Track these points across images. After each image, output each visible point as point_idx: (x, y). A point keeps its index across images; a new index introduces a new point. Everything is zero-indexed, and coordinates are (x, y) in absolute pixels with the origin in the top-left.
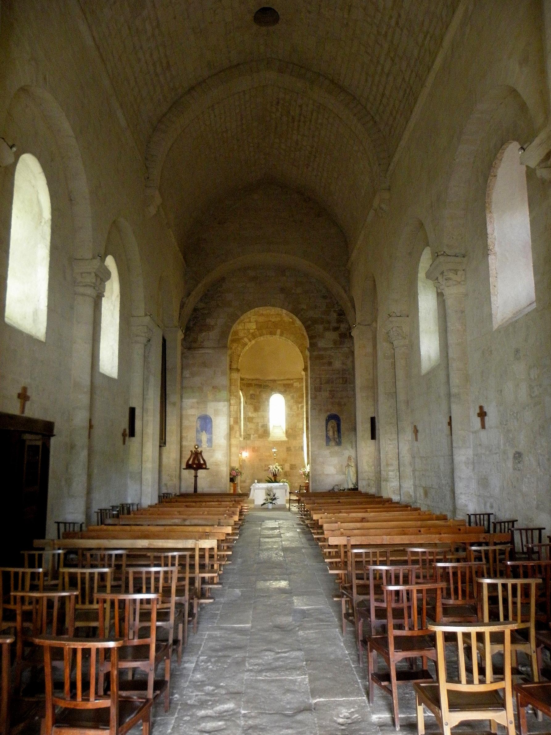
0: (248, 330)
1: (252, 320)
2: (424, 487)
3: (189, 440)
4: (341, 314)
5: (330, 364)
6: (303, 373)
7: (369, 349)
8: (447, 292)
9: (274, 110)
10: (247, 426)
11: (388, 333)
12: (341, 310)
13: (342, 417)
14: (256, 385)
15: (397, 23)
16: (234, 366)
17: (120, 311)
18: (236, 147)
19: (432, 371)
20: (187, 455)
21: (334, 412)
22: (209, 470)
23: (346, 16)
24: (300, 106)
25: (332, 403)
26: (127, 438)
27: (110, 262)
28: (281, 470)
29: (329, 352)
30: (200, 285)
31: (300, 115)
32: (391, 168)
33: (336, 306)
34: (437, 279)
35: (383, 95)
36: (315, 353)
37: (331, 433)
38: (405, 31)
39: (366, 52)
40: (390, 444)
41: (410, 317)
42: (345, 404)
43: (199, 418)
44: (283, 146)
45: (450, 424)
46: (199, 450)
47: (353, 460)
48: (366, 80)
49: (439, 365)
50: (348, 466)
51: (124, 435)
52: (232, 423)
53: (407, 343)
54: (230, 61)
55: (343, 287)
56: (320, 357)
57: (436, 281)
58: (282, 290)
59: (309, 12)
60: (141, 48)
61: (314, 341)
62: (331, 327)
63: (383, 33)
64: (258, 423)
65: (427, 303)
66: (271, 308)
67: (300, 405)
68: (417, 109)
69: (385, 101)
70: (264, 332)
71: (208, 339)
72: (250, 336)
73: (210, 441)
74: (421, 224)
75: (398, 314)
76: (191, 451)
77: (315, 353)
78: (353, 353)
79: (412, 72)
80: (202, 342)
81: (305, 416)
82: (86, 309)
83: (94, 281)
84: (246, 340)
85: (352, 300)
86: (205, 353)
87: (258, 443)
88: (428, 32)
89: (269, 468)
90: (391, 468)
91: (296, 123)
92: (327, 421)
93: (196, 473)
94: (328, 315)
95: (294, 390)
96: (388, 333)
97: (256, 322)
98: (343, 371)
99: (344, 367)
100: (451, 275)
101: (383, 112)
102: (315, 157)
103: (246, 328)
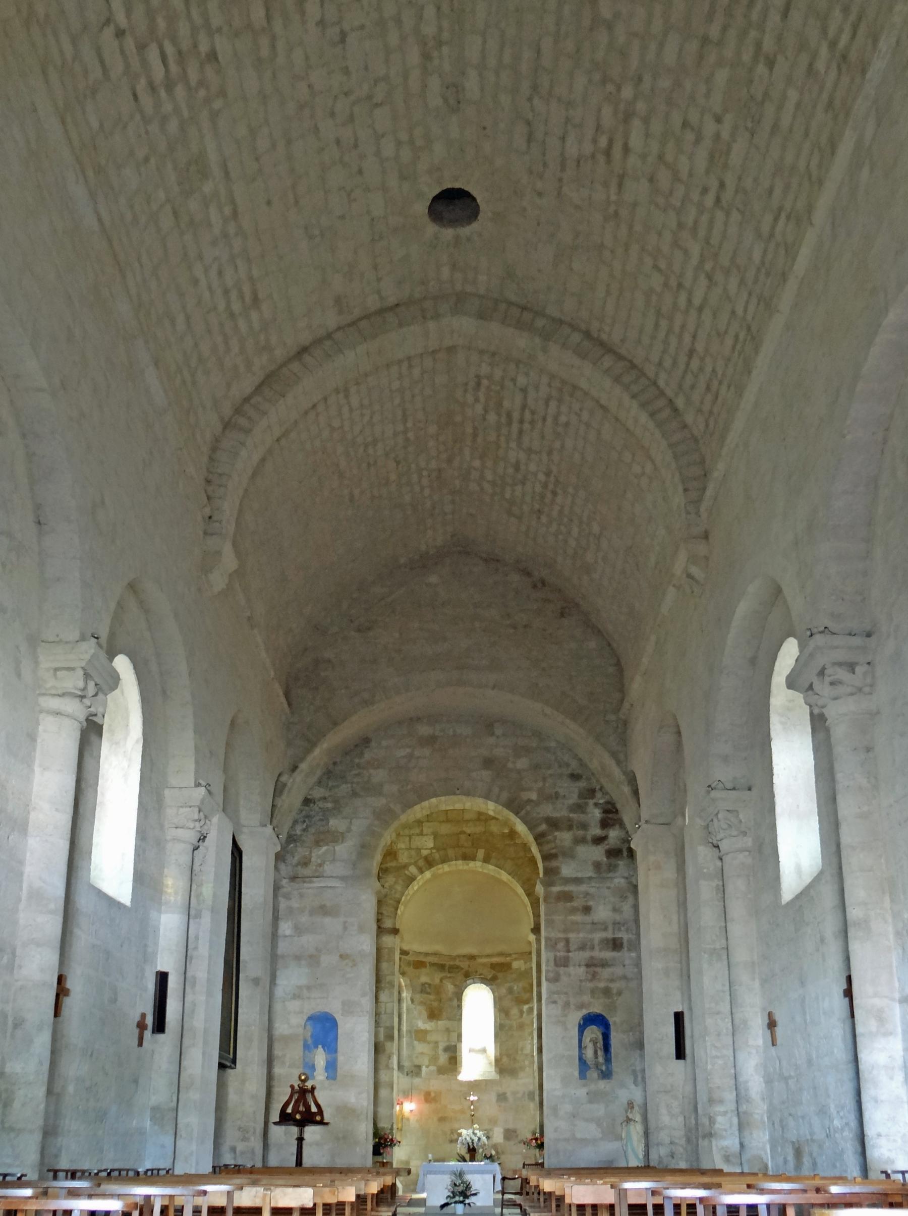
0: (418, 850)
1: (425, 831)
2: (793, 1143)
3: (287, 1064)
4: (611, 815)
5: (587, 910)
6: (532, 937)
7: (670, 873)
8: (833, 711)
9: (470, 399)
10: (413, 1047)
11: (707, 826)
12: (608, 803)
13: (614, 1020)
14: (433, 965)
15: (718, 200)
16: (388, 924)
17: (141, 770)
18: (393, 477)
19: (806, 894)
20: (282, 1095)
21: (597, 1009)
22: (330, 1126)
23: (613, 198)
24: (524, 391)
25: (593, 992)
26: (148, 1034)
27: (122, 664)
28: (484, 1139)
29: (583, 888)
30: (317, 752)
31: (524, 407)
32: (709, 492)
33: (599, 795)
34: (811, 687)
35: (691, 353)
36: (556, 889)
37: (589, 1053)
38: (735, 216)
39: (656, 267)
40: (717, 1057)
41: (755, 791)
42: (619, 993)
43: (310, 1018)
44: (489, 476)
45: (848, 993)
46: (309, 1084)
47: (636, 1108)
48: (657, 325)
49: (821, 873)
50: (628, 1120)
51: (141, 1026)
52: (382, 1037)
53: (750, 844)
54: (381, 298)
55: (614, 755)
56: (567, 897)
57: (810, 692)
58: (488, 763)
59: (540, 194)
60: (200, 257)
61: (554, 864)
62: (589, 838)
63: (690, 223)
64: (436, 1043)
65: (792, 760)
66: (464, 798)
67: (526, 1007)
68: (762, 363)
69: (695, 364)
70: (451, 852)
71: (334, 860)
72: (421, 863)
73: (331, 1067)
74: (778, 592)
75: (729, 786)
76: (292, 1087)
77: (556, 889)
78: (635, 889)
79: (750, 294)
80: (320, 865)
81: (535, 1026)
82: (58, 740)
83: (81, 684)
84: (413, 870)
85: (632, 780)
86: (327, 887)
87: (437, 1084)
88: (780, 209)
89: (460, 1135)
90: (720, 1108)
91: (515, 427)
92: (582, 1029)
93: (301, 1132)
94: (584, 812)
95: (514, 976)
96: (707, 826)
97: (436, 836)
98: (614, 924)
99: (618, 918)
100: (842, 674)
101: (693, 387)
102: (554, 493)
103: (413, 846)
